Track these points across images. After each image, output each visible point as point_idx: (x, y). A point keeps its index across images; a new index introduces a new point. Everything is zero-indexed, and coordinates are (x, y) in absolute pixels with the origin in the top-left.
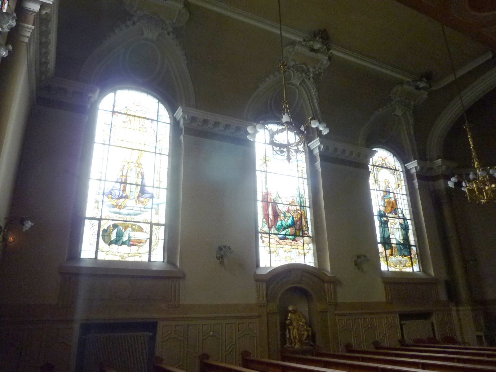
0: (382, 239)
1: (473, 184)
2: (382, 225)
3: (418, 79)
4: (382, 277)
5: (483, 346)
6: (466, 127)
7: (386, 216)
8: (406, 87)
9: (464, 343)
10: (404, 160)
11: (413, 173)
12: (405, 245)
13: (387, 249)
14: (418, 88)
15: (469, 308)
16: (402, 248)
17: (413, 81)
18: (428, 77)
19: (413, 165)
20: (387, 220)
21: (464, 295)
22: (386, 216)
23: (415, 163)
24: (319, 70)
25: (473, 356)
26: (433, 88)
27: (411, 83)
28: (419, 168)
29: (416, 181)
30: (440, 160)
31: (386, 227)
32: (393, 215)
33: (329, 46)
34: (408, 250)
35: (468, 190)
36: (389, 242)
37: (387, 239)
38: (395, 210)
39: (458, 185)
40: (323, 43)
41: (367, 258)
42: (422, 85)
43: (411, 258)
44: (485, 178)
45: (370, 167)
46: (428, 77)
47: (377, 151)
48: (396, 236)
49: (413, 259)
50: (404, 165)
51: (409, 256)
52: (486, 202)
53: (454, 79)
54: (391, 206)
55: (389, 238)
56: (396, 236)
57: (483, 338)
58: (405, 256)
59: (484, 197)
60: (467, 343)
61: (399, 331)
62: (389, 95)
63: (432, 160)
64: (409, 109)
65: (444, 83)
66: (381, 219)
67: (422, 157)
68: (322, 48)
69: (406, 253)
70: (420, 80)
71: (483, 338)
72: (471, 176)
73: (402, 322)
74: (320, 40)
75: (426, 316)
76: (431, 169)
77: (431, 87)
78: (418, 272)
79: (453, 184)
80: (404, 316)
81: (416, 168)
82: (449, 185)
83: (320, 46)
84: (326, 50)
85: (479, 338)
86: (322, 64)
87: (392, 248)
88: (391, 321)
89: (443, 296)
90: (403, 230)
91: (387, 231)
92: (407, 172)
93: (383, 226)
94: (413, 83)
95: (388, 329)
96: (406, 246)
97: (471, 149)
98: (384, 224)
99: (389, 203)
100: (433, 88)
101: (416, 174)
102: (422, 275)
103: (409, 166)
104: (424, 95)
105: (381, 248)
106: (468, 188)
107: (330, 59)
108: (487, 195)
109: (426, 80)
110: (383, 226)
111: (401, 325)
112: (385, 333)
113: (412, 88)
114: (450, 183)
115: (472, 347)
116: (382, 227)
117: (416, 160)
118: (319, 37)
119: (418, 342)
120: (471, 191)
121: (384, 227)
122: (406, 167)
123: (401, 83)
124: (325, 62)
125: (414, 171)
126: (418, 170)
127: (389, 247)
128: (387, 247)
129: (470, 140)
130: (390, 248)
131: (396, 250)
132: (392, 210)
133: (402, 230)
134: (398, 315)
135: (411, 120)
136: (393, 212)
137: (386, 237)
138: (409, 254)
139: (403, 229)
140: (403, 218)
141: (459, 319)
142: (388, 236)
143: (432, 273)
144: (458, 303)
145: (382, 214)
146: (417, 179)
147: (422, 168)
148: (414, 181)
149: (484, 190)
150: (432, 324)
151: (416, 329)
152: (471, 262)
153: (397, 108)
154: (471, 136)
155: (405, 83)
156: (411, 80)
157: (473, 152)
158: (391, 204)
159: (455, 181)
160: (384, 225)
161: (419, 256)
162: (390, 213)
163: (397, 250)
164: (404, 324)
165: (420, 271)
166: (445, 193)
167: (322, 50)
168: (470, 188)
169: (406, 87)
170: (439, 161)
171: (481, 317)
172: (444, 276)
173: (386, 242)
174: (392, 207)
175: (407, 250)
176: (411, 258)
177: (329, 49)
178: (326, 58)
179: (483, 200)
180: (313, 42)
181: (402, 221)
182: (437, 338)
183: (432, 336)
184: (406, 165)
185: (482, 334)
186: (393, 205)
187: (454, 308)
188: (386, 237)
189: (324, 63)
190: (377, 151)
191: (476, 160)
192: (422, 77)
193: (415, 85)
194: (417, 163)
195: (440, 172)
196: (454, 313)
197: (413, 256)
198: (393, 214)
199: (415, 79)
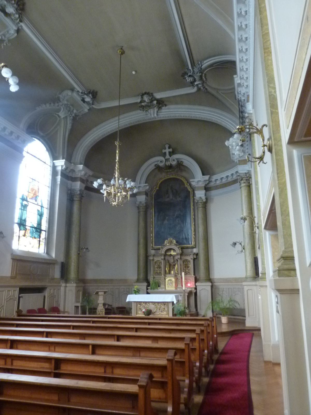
0: (19, 220)
1: (112, 189)
2: (22, 207)
3: (86, 93)
4: (12, 254)
5: (78, 314)
6: (117, 143)
7: (27, 201)
8: (75, 94)
9: (64, 312)
10: (54, 157)
11: (58, 170)
12: (38, 229)
13: (22, 230)
14: (83, 100)
15: (75, 285)
16: (34, 231)
17: (82, 93)
18: (94, 95)
19: (61, 163)
20: (28, 204)
21: (73, 274)
22: (27, 201)
23: (62, 162)
24: (3, 37)
25: (46, 328)
26: (94, 106)
27: (80, 94)
28: (64, 167)
29: (59, 178)
30: (82, 165)
31: (25, 211)
32: (34, 201)
33: (22, 17)
34: (39, 233)
35: (107, 192)
36: (24, 224)
37: (23, 221)
38: (36, 197)
39: (101, 186)
40: (17, 9)
41: (3, 235)
42: (88, 99)
43: (40, 241)
44: (121, 186)
45: (24, 153)
46: (94, 95)
47: (35, 140)
48: (32, 221)
49: (41, 242)
50: (53, 161)
51: (38, 239)
52: (117, 205)
53: (118, 104)
54: (33, 193)
55: (25, 220)
56: (32, 221)
57: (80, 308)
58: (35, 238)
59: (116, 200)
60: (67, 312)
61: (16, 303)
62: (59, 96)
63: (75, 164)
64: (71, 115)
65: (104, 105)
66: (22, 202)
67: (69, 159)
68: (14, 15)
69: (36, 236)
70: (87, 95)
71: (80, 308)
72: (112, 182)
73: (21, 295)
74: (15, 5)
75: (40, 290)
76: (73, 171)
77: (93, 104)
78: (43, 254)
79: (98, 184)
80: (23, 290)
81: (62, 166)
82: (94, 185)
83: (13, 11)
84: (17, 19)
85: (77, 307)
86: (8, 32)
87: (26, 230)
88: (11, 294)
89: (57, 274)
90: (38, 216)
91: (25, 214)
92: (54, 167)
93: (22, 208)
94: (82, 94)
95: (7, 301)
96: (38, 230)
97: (116, 162)
98: (24, 207)
99: (33, 190)
100: (94, 106)
101: (61, 172)
102: (46, 256)
103: (57, 163)
104: (86, 108)
105: (16, 227)
106: (107, 190)
107: (18, 31)
108: (118, 200)
109: (91, 97)
110: (22, 208)
111: (19, 298)
112: (3, 305)
113: (79, 99)
114: (96, 183)
115: (71, 315)
116: (22, 209)
117: (64, 160)
118: (15, 2)
119: (31, 312)
120: (109, 194)
121: (23, 210)
122: (54, 163)
123: (73, 90)
124: (12, 32)
125: (59, 169)
126: (63, 168)
127: (23, 229)
128: (22, 227)
129: (117, 155)
130: (24, 229)
131: (29, 232)
132: (34, 197)
133: (38, 215)
134: (18, 289)
135: (69, 126)
136: (34, 198)
137: (23, 219)
138: (39, 237)
139: (39, 215)
140: (41, 205)
141: (65, 292)
142: (24, 219)
143: (54, 255)
144: (67, 281)
145: (24, 198)
146: (61, 176)
147: (66, 169)
148: (57, 177)
149: (117, 196)
150: (45, 297)
151: (31, 302)
152: (85, 250)
153: (62, 111)
154: (119, 152)
155: (76, 91)
156: (81, 91)
157: (117, 164)
158: (34, 191)
159: (100, 183)
160: (24, 208)
161: (46, 239)
162: (32, 198)
163: (30, 232)
164: (22, 297)
165: (44, 253)
166: (78, 192)
167: (13, 18)
168: (109, 191)
169: (75, 94)
170: (81, 167)
171: (81, 292)
172: (61, 259)
173: (22, 224)
174: (34, 194)
175: (38, 233)
176: (40, 241)
177: (21, 21)
178: (15, 28)
179: (115, 203)
180: (7, 3)
181: (39, 208)
182: (46, 308)
183: (42, 307)
184: (54, 161)
185: (79, 305)
186: (35, 192)
187: (63, 285)
188: (23, 219)
189: (10, 32)
190: (35, 140)
191: (117, 171)
192: (89, 93)
193: (82, 96)
194: (64, 162)
195: (79, 175)
196: (62, 289)
197: (41, 239)
198: (34, 200)
199: (84, 92)
